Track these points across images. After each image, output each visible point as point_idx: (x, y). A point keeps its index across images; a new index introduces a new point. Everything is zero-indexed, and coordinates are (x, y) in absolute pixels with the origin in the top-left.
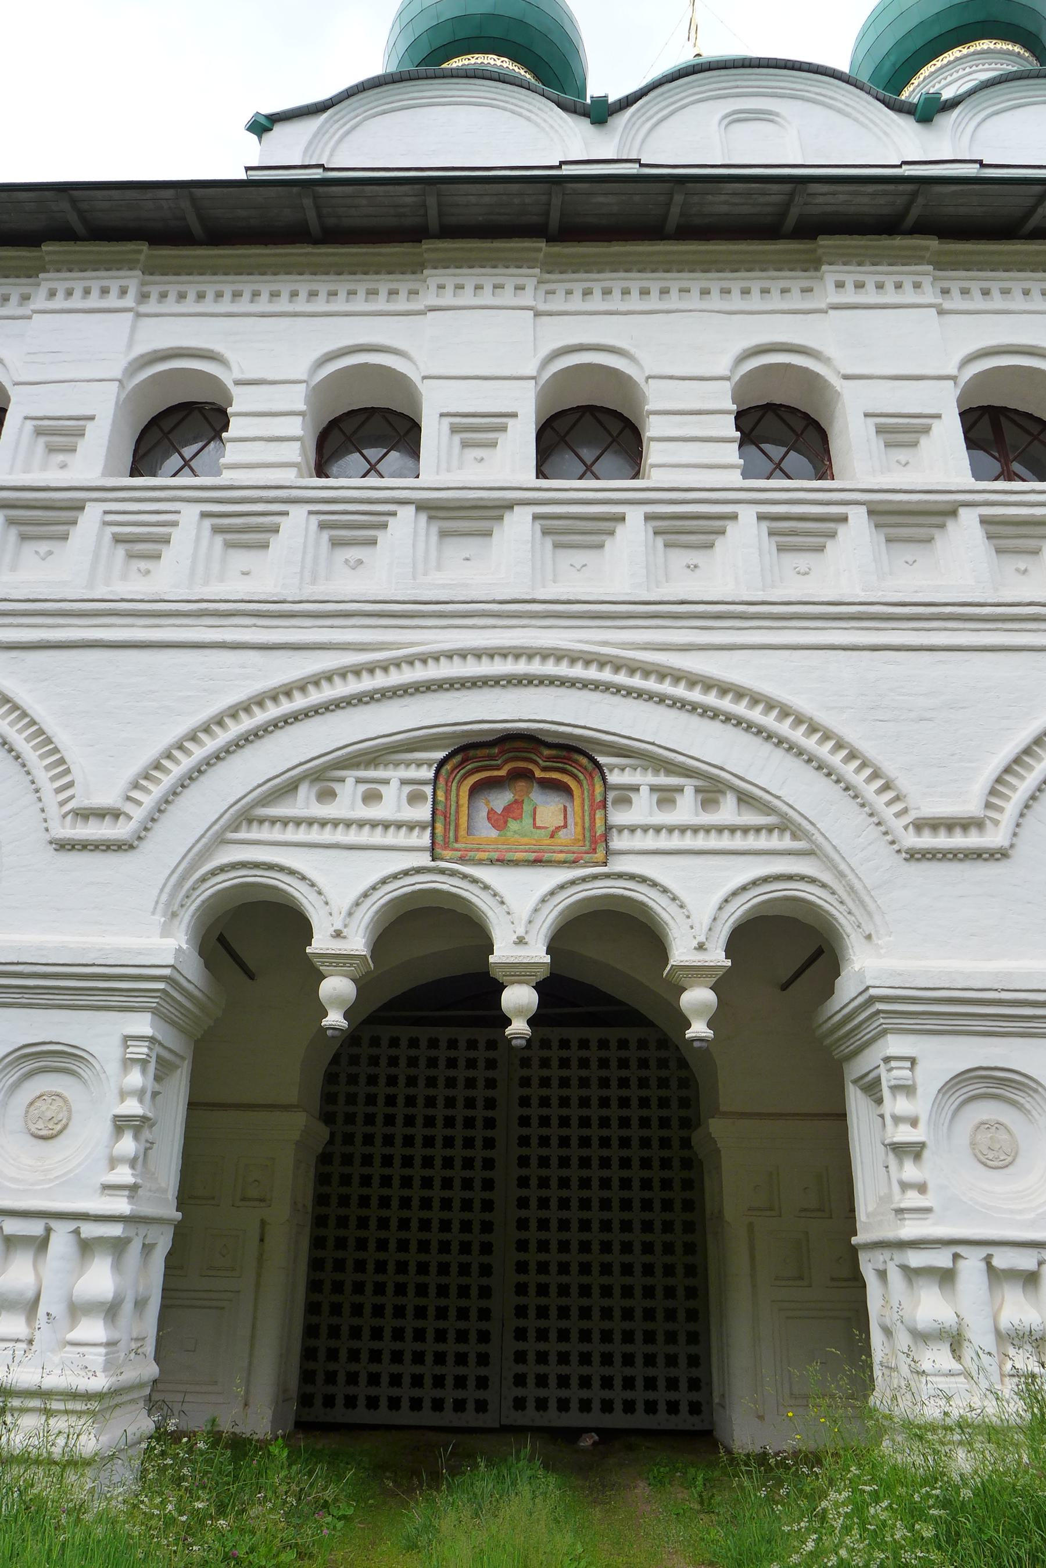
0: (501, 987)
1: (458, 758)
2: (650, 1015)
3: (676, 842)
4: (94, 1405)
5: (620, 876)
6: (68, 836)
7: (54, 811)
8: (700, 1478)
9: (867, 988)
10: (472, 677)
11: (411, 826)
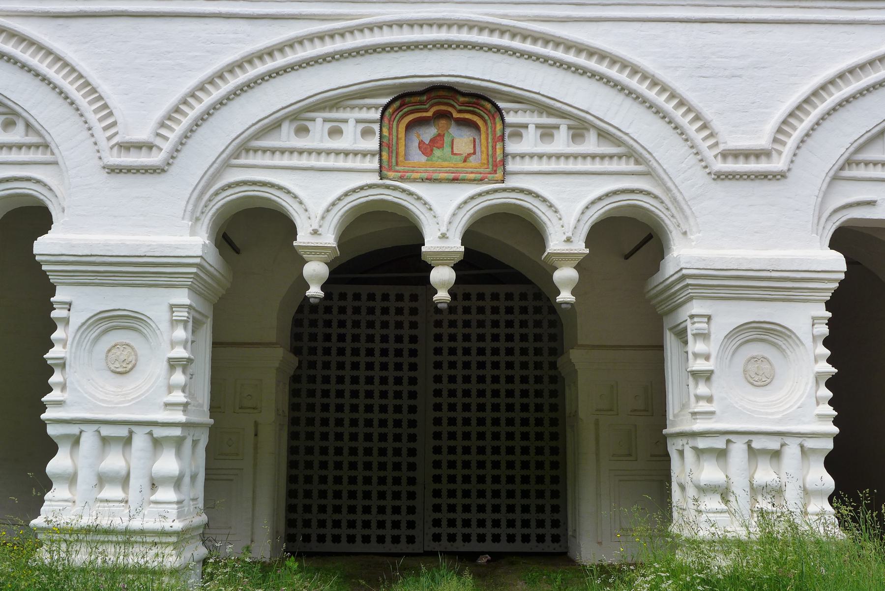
0: (430, 268)
1: (397, 104)
2: (530, 276)
3: (553, 166)
4: (174, 539)
5: (513, 190)
6: (117, 163)
7: (104, 145)
8: (559, 577)
9: (681, 269)
10: (407, 43)
11: (364, 154)
